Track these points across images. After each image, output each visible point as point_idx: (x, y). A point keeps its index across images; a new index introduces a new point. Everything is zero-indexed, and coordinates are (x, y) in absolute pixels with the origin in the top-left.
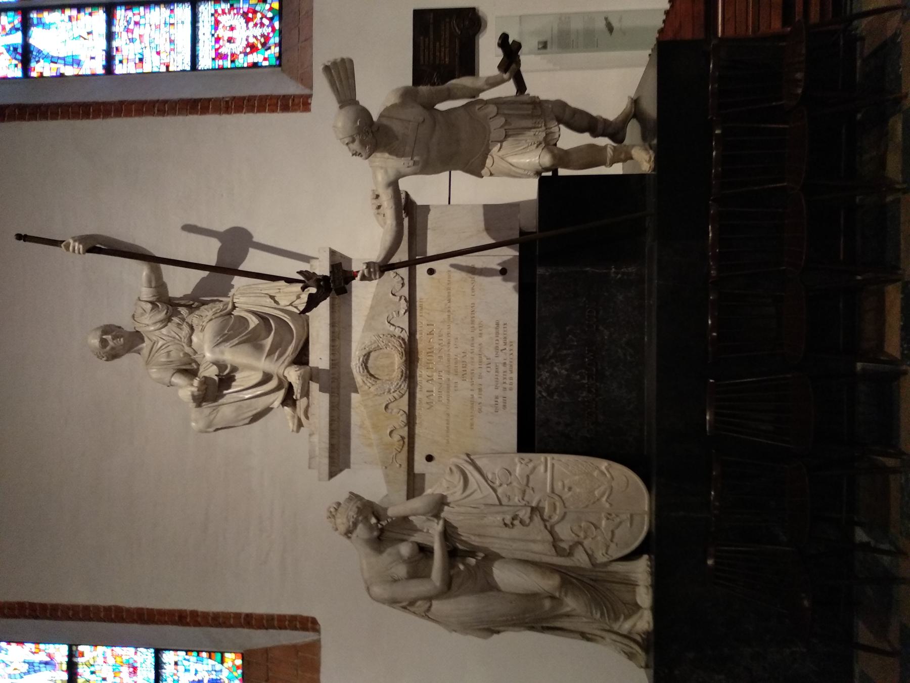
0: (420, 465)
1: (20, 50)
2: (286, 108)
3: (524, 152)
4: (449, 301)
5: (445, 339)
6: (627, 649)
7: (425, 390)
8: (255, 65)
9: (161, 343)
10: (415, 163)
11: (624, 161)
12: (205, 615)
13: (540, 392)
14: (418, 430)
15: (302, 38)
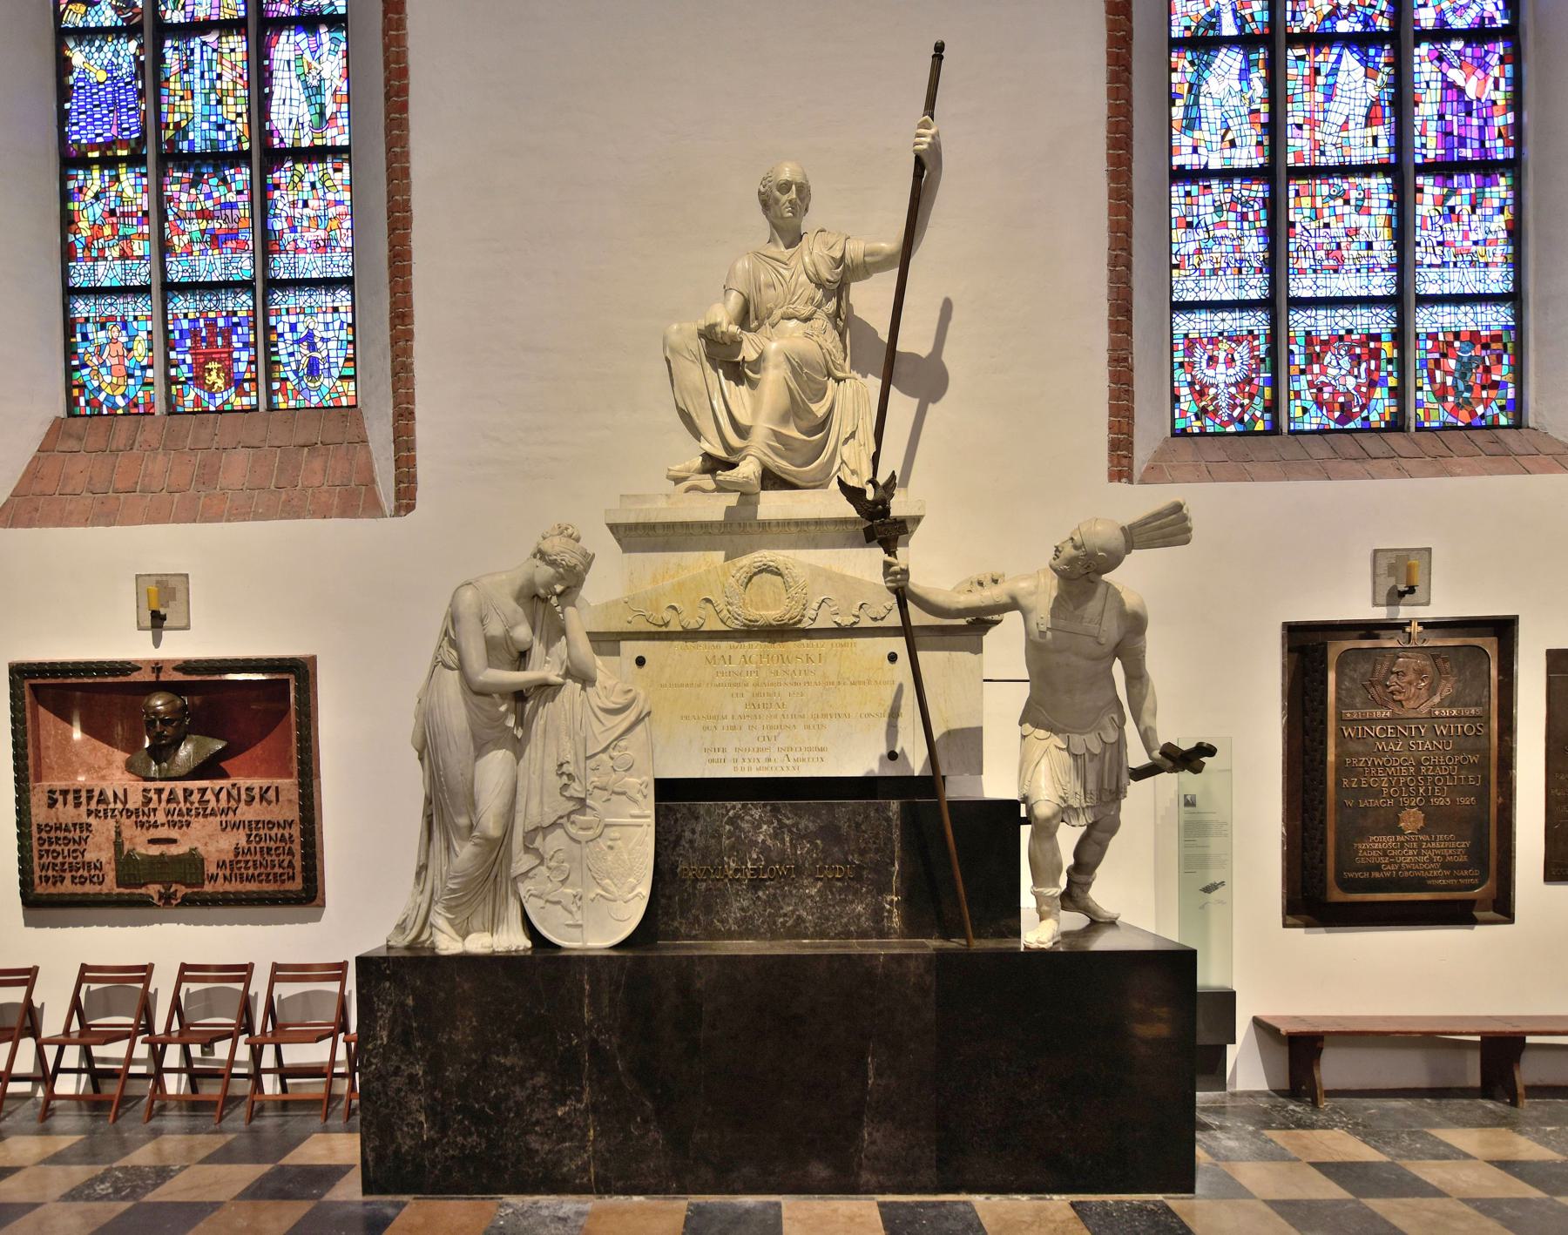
0: (630, 649)
1: (1211, 33)
2: (1114, 446)
3: (1054, 779)
4: (853, 684)
5: (801, 678)
6: (409, 924)
7: (731, 652)
8: (1176, 399)
9: (786, 273)
10: (1042, 634)
11: (1038, 909)
12: (408, 352)
13: (734, 807)
14: (678, 645)
15: (1212, 467)
